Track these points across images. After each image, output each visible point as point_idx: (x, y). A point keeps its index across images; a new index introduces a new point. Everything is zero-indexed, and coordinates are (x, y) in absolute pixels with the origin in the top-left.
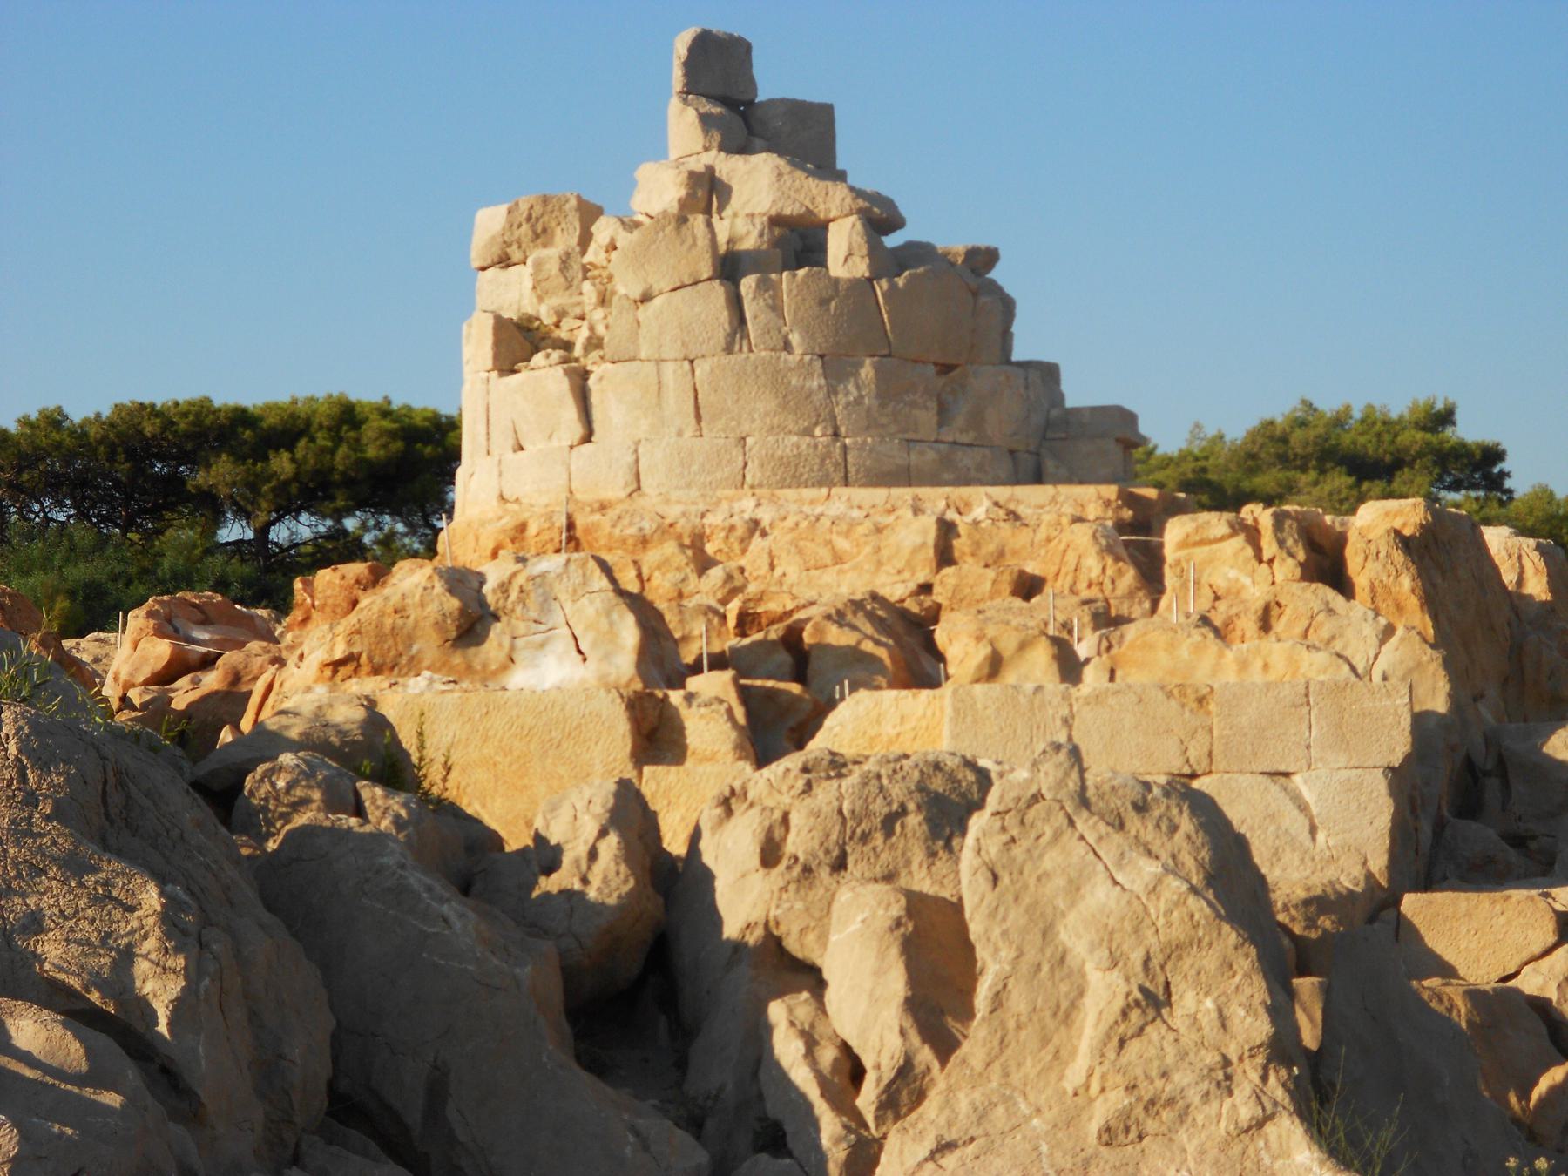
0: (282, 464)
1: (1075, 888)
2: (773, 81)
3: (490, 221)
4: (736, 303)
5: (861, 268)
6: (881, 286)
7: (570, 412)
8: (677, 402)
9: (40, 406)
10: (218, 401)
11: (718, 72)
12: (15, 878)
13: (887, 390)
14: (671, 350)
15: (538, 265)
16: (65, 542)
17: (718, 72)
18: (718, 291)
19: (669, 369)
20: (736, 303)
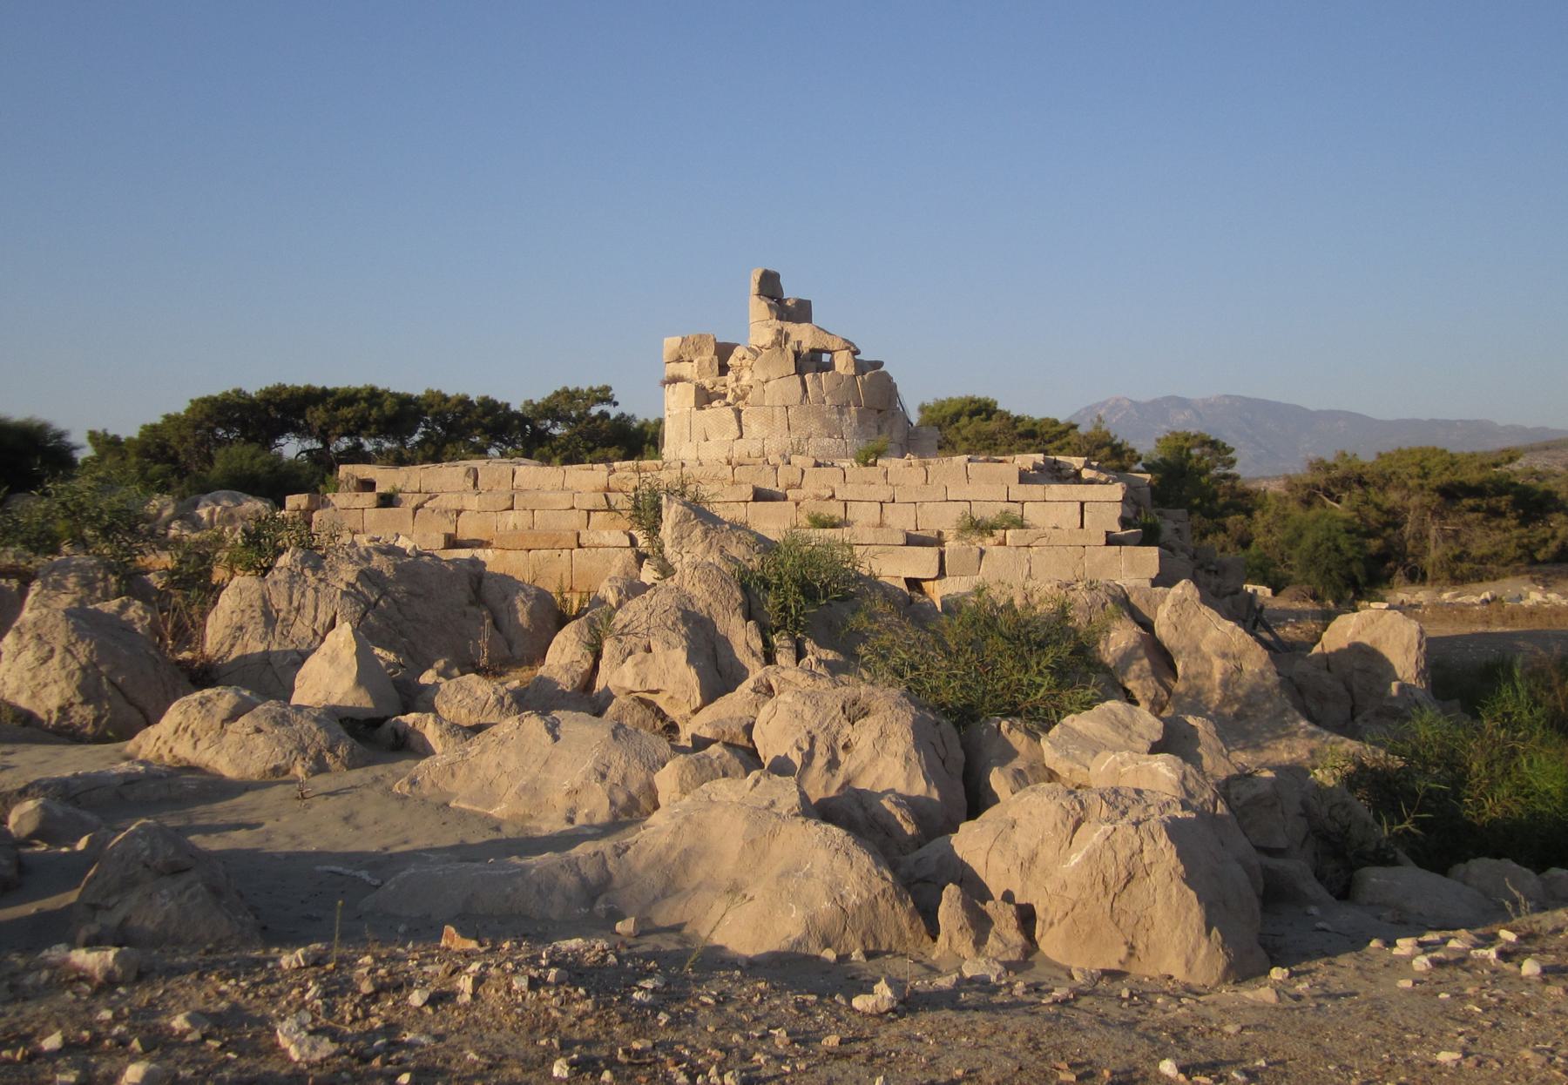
0: (346, 412)
1: (1204, 632)
2: (791, 293)
3: (671, 343)
4: (804, 383)
5: (852, 371)
6: (859, 379)
7: (735, 426)
8: (780, 422)
9: (484, 394)
10: (955, 396)
11: (770, 286)
12: (794, 1068)
13: (861, 421)
14: (779, 402)
15: (700, 363)
16: (1103, 985)
17: (770, 286)
18: (797, 379)
19: (777, 410)
20: (804, 383)
